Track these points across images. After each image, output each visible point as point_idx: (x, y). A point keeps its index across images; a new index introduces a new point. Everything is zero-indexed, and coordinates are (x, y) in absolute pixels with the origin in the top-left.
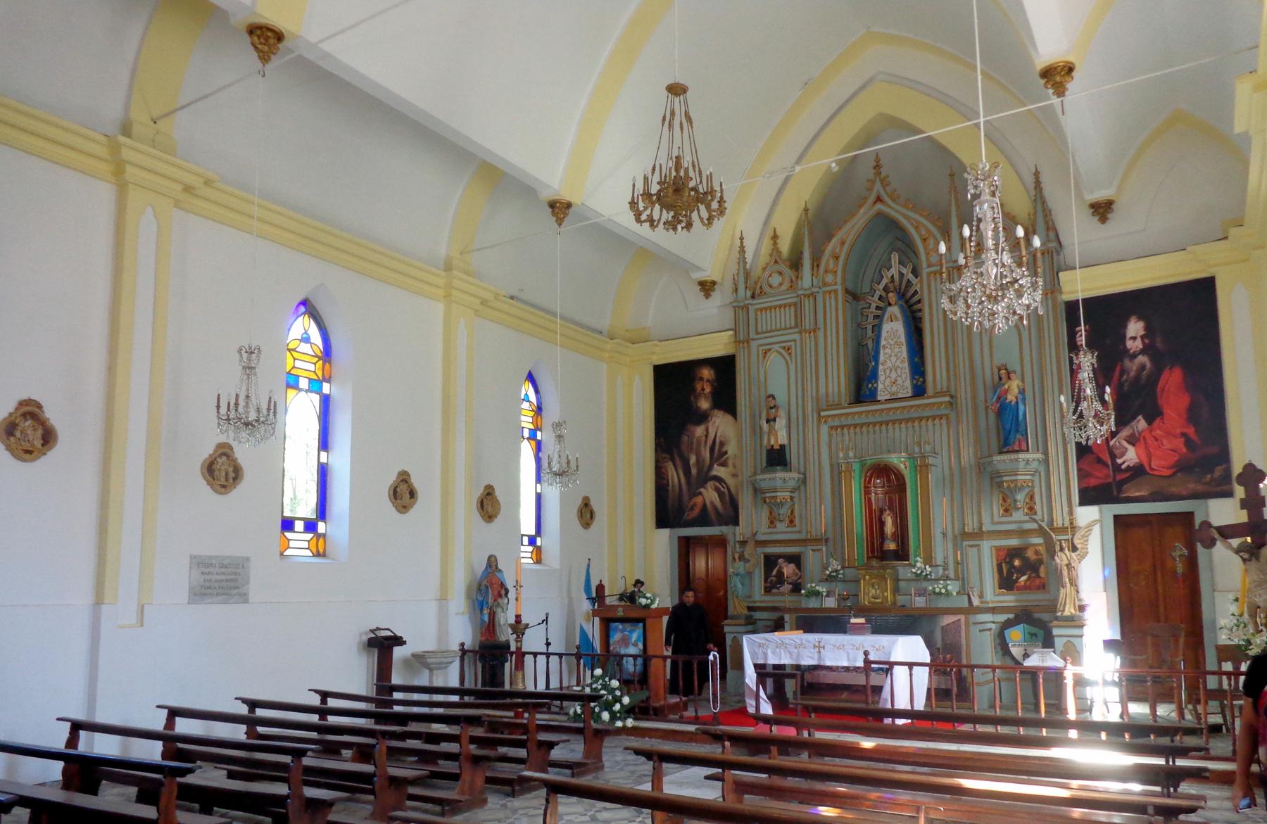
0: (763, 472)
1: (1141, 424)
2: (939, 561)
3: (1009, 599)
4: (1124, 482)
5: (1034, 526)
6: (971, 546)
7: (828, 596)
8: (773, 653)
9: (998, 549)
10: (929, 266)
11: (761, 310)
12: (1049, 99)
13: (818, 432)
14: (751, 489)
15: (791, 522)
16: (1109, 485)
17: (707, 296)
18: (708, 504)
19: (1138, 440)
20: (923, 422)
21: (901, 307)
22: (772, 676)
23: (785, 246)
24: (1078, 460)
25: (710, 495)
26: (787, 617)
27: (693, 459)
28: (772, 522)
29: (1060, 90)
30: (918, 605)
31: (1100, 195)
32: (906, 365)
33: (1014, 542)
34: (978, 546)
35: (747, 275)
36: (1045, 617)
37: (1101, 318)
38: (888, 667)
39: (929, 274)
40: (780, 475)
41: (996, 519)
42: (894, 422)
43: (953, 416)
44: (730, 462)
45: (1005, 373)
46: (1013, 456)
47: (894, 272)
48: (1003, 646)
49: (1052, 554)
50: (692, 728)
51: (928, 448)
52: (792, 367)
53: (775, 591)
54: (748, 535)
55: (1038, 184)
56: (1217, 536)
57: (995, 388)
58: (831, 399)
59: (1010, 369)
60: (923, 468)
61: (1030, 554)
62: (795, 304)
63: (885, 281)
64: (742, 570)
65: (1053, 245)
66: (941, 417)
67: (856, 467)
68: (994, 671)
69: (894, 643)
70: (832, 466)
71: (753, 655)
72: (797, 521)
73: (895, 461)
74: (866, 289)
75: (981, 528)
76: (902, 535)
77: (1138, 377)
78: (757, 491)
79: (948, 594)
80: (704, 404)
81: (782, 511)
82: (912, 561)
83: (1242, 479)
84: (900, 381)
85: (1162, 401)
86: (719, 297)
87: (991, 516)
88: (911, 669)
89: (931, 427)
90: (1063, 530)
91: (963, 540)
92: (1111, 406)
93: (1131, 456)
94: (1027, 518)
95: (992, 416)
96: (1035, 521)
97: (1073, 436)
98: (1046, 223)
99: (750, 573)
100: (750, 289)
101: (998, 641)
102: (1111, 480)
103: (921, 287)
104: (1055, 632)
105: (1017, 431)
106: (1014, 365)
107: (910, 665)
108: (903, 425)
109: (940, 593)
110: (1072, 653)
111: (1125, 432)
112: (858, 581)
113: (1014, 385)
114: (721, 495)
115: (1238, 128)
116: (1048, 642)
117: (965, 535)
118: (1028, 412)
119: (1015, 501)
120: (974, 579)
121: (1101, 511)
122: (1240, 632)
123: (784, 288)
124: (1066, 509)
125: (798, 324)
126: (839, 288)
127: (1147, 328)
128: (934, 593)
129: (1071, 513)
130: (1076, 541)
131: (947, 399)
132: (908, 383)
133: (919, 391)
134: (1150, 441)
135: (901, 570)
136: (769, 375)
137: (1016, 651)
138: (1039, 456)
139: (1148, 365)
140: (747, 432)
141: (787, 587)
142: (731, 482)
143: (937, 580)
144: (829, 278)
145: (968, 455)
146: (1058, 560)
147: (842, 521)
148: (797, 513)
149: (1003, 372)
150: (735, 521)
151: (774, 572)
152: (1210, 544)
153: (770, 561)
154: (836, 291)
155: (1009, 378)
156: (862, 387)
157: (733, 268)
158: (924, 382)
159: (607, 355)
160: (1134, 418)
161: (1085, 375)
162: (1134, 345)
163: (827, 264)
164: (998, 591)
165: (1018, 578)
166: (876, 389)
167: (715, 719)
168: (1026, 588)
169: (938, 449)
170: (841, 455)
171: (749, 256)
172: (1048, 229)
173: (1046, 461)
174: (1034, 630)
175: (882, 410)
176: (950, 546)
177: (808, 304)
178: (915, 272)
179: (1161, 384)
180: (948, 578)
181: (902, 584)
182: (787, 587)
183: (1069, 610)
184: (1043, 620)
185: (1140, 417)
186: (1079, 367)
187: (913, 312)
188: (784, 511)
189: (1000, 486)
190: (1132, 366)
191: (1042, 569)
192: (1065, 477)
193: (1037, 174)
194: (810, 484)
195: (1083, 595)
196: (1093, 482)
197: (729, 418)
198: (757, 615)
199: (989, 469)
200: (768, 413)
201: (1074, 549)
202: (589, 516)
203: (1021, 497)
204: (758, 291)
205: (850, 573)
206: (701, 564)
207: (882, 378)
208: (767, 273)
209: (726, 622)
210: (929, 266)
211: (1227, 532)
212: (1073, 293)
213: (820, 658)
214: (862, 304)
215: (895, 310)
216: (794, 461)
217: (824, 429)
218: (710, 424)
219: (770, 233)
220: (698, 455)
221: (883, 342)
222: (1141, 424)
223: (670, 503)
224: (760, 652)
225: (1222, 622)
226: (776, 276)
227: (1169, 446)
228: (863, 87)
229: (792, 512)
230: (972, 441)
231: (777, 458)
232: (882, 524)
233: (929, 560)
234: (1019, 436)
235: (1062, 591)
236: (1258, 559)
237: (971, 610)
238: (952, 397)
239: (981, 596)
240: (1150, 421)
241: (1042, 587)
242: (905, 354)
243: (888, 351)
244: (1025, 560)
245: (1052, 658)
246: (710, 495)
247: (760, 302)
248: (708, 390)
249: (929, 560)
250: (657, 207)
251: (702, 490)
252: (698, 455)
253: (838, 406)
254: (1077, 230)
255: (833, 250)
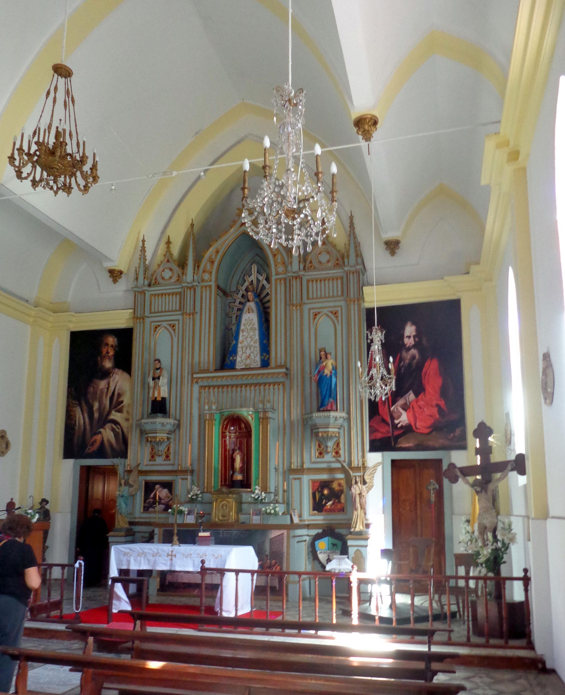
0: (148, 417)
1: (411, 396)
2: (272, 489)
3: (320, 518)
4: (399, 436)
5: (338, 465)
6: (295, 479)
7: (189, 514)
8: (135, 560)
9: (314, 482)
10: (277, 274)
11: (155, 295)
12: (359, 142)
13: (191, 391)
14: (138, 431)
15: (167, 457)
16: (389, 438)
17: (115, 281)
18: (105, 439)
19: (409, 408)
20: (267, 387)
21: (257, 303)
22: (136, 581)
23: (176, 250)
24: (370, 420)
25: (107, 434)
26: (157, 531)
27: (96, 405)
28: (153, 457)
29: (367, 137)
30: (254, 522)
31: (391, 235)
32: (257, 345)
33: (324, 477)
34: (300, 479)
35: (146, 269)
36: (343, 531)
37: (389, 319)
38: (222, 572)
39: (276, 280)
40: (160, 420)
41: (313, 460)
42: (246, 385)
43: (287, 383)
44: (125, 410)
45: (323, 355)
46: (326, 414)
47: (253, 278)
48: (313, 553)
49: (350, 486)
50: (61, 627)
51: (268, 405)
52: (175, 340)
53: (151, 509)
54: (134, 465)
55: (352, 225)
56: (459, 474)
57: (317, 365)
58: (202, 365)
59: (327, 352)
60: (264, 420)
61: (335, 486)
62: (180, 293)
63: (246, 284)
64: (126, 494)
65: (359, 267)
66: (279, 384)
67: (217, 417)
68: (300, 576)
69: (229, 553)
70: (200, 416)
71: (119, 562)
72: (171, 457)
73: (245, 414)
74: (234, 289)
75: (302, 466)
76: (246, 469)
77: (410, 364)
78: (142, 432)
79: (276, 514)
80: (108, 364)
81: (160, 449)
82: (253, 489)
83: (476, 434)
84: (252, 356)
85: (425, 382)
86: (123, 285)
87: (310, 457)
88: (237, 575)
89: (272, 390)
90: (357, 469)
91: (290, 474)
92: (393, 372)
93: (404, 419)
94: (334, 459)
95: (314, 385)
96: (339, 462)
97: (366, 396)
98: (356, 251)
99: (133, 496)
100: (147, 281)
101: (310, 550)
102: (390, 435)
103: (271, 291)
104: (350, 543)
105: (330, 396)
106: (330, 348)
107: (237, 572)
108: (252, 388)
109: (270, 513)
110: (359, 562)
111: (401, 402)
112: (211, 503)
113: (329, 363)
114: (116, 435)
115: (484, 181)
116: (344, 551)
117: (292, 471)
118: (338, 383)
119: (327, 447)
120: (295, 504)
121: (383, 456)
122: (473, 545)
123: (173, 280)
124: (360, 454)
125: (181, 308)
126: (213, 284)
127: (417, 330)
128: (267, 513)
129: (363, 456)
130: (366, 477)
131: (284, 370)
132: (258, 359)
133: (265, 364)
134: (417, 409)
135: (244, 495)
136: (158, 345)
137: (322, 557)
138: (344, 415)
139: (417, 356)
140: (138, 388)
141: (159, 507)
142: (124, 424)
143: (269, 503)
144: (206, 276)
145: (296, 413)
146: (353, 490)
147: (204, 457)
148: (172, 450)
149: (323, 353)
150: (124, 455)
151: (152, 495)
152: (454, 480)
153: (149, 487)
154: (210, 286)
155: (326, 358)
156: (226, 359)
157: (136, 262)
158: (269, 358)
159: (31, 319)
160: (407, 392)
161: (376, 347)
162: (409, 342)
163: (205, 266)
164: (312, 512)
165: (326, 503)
166: (235, 361)
167: (78, 618)
168: (331, 511)
169: (276, 407)
170: (207, 407)
171: (149, 255)
172: (357, 256)
173: (349, 419)
174: (336, 541)
175: (238, 376)
176: (281, 478)
177: (189, 293)
178: (268, 279)
179: (424, 370)
180: (277, 502)
181: (244, 506)
182: (159, 507)
183: (359, 527)
184: (340, 536)
185: (411, 392)
186: (372, 341)
187: (263, 304)
188: (162, 448)
189: (316, 435)
190: (407, 356)
191: (343, 497)
192: (361, 430)
193: (351, 218)
194: (183, 429)
195: (369, 516)
196: (379, 436)
197: (126, 375)
198: (136, 528)
199: (310, 422)
200: (154, 373)
201: (364, 483)
202: (4, 446)
203: (330, 444)
204: (153, 281)
205: (207, 496)
206: (99, 488)
207: (240, 353)
208: (161, 268)
209: (111, 533)
210: (277, 274)
211: (466, 471)
212: (371, 302)
213: (171, 565)
214: (230, 299)
215: (252, 305)
216: (172, 411)
217: (196, 388)
218: (112, 379)
219: (165, 240)
220: (100, 403)
221: (242, 327)
222: (411, 396)
223: (75, 441)
224: (124, 559)
225: (490, 551)
226: (167, 271)
227: (428, 413)
228: (239, 142)
229: (168, 450)
230: (299, 403)
231: (159, 407)
232: (233, 460)
233: (265, 489)
234: (331, 400)
235: (355, 513)
236: (486, 492)
237: (292, 526)
238: (287, 369)
239: (300, 516)
240: (417, 394)
241: (342, 510)
242: (257, 337)
243: (245, 334)
244: (331, 490)
245: (346, 563)
246: (107, 434)
247: (155, 290)
248: (111, 353)
249: (265, 489)
250: (39, 169)
251: (102, 430)
252: (100, 403)
253: (207, 371)
254: (375, 259)
255: (210, 257)
